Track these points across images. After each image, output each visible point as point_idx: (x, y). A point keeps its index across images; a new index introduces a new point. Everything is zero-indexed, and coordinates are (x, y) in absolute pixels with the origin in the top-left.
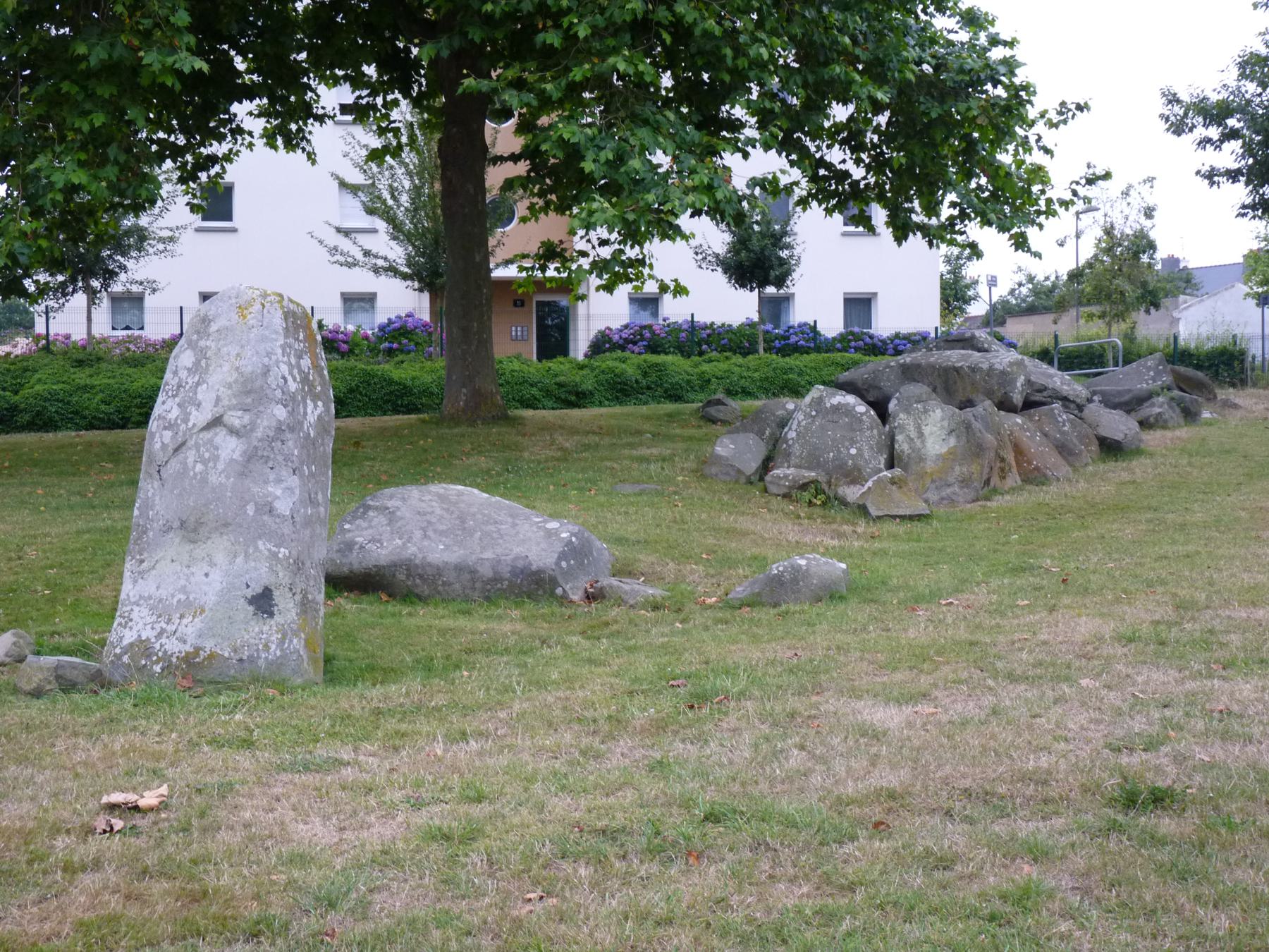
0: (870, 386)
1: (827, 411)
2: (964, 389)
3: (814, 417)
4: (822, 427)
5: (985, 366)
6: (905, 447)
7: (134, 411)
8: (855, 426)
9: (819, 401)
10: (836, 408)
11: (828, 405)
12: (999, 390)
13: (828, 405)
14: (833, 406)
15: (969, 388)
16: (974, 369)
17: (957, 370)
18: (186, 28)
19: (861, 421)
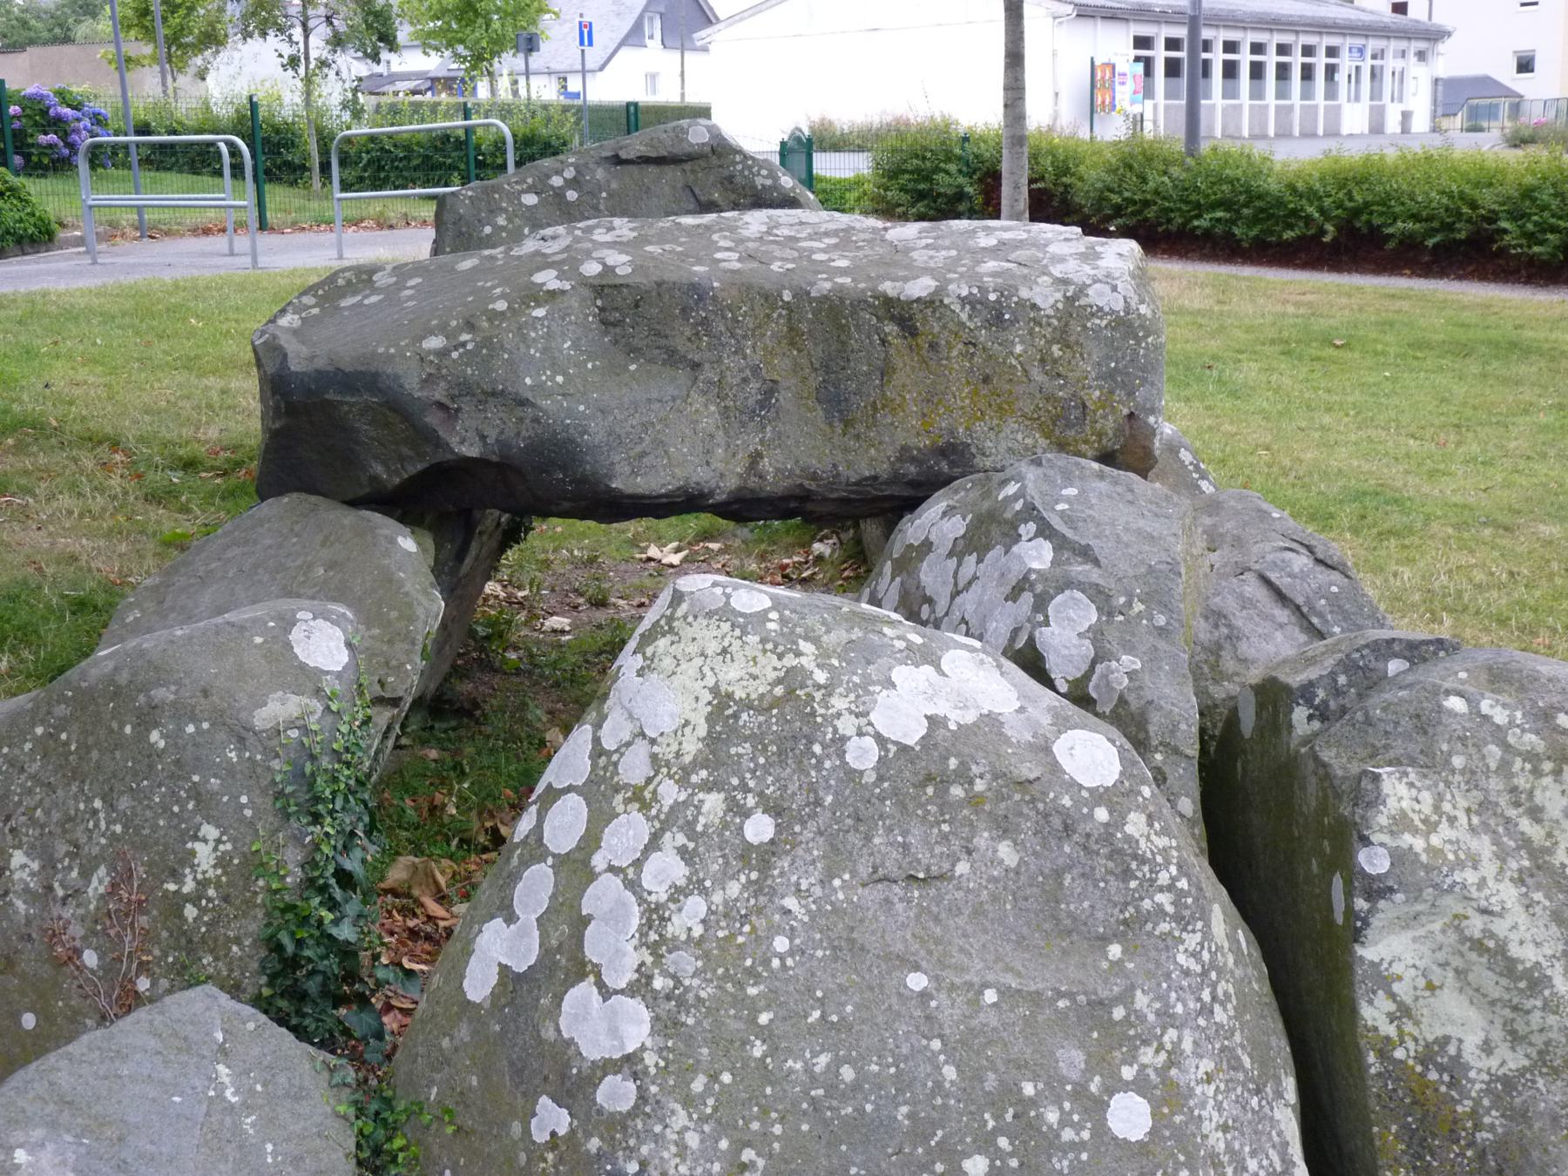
0: (464, 389)
1: (860, 806)
2: (931, 398)
3: (764, 856)
4: (843, 938)
5: (1045, 296)
6: (1462, 1024)
7: (710, 22)
8: (1080, 902)
9: (772, 736)
10: (931, 770)
11: (863, 755)
12: (1106, 402)
13: (863, 755)
14: (895, 756)
15: (961, 396)
16: (998, 313)
17: (902, 315)
18: (457, 579)
19: (1124, 859)
